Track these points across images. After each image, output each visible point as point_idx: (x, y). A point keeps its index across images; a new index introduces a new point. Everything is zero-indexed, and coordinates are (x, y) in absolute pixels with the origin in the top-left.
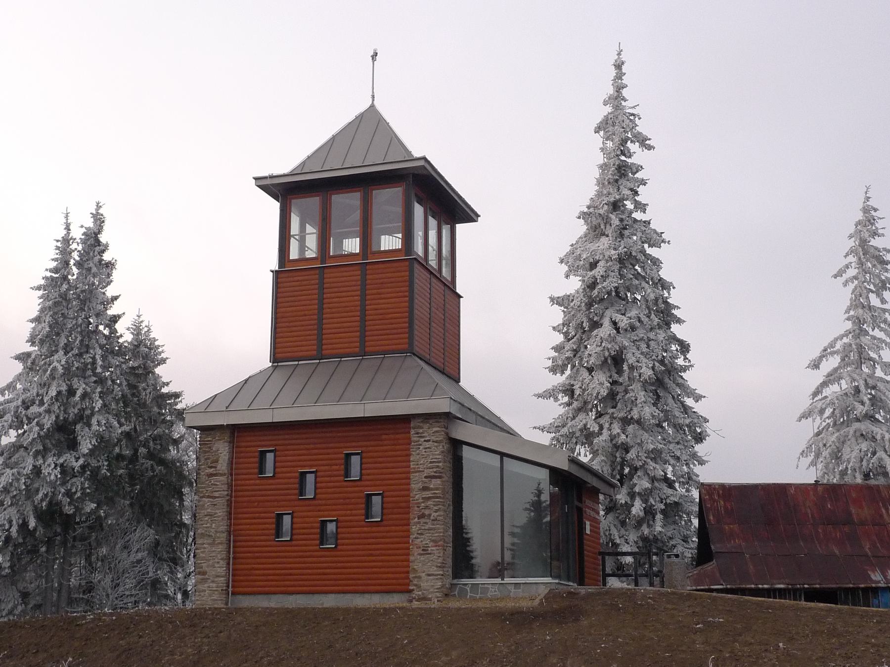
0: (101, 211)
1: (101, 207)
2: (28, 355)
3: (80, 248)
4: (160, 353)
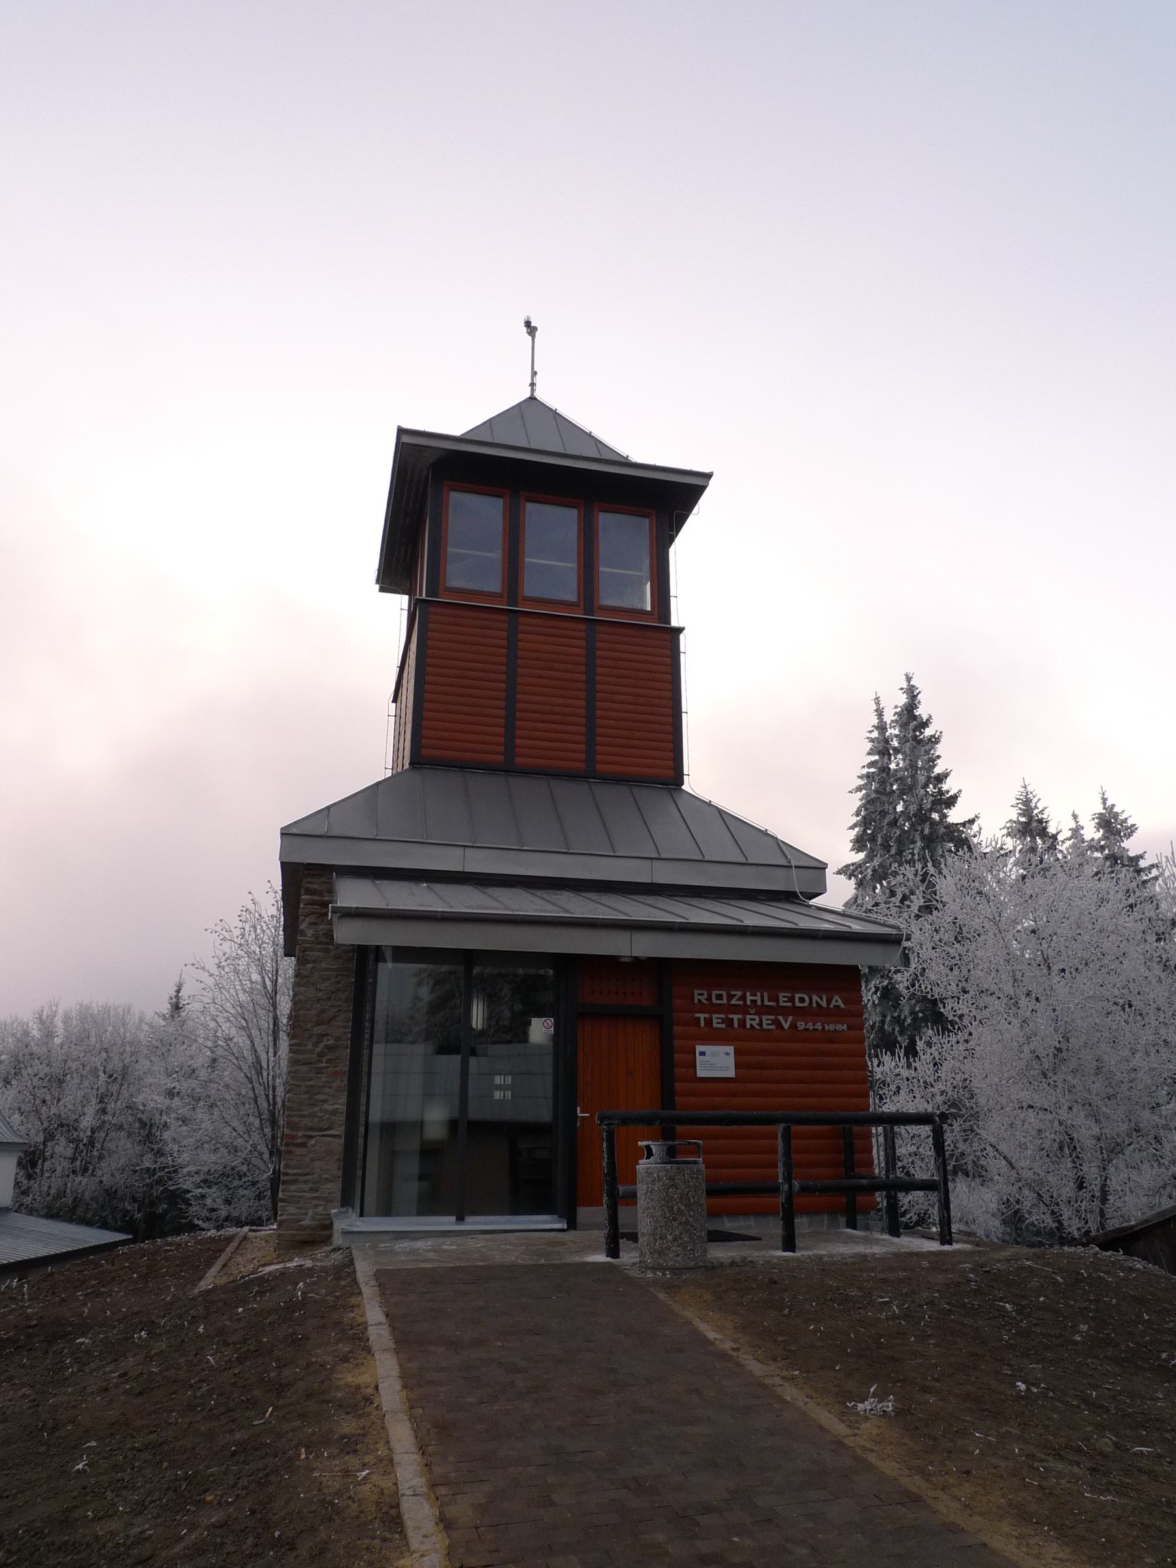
0: (912, 683)
1: (911, 678)
2: (1129, 836)
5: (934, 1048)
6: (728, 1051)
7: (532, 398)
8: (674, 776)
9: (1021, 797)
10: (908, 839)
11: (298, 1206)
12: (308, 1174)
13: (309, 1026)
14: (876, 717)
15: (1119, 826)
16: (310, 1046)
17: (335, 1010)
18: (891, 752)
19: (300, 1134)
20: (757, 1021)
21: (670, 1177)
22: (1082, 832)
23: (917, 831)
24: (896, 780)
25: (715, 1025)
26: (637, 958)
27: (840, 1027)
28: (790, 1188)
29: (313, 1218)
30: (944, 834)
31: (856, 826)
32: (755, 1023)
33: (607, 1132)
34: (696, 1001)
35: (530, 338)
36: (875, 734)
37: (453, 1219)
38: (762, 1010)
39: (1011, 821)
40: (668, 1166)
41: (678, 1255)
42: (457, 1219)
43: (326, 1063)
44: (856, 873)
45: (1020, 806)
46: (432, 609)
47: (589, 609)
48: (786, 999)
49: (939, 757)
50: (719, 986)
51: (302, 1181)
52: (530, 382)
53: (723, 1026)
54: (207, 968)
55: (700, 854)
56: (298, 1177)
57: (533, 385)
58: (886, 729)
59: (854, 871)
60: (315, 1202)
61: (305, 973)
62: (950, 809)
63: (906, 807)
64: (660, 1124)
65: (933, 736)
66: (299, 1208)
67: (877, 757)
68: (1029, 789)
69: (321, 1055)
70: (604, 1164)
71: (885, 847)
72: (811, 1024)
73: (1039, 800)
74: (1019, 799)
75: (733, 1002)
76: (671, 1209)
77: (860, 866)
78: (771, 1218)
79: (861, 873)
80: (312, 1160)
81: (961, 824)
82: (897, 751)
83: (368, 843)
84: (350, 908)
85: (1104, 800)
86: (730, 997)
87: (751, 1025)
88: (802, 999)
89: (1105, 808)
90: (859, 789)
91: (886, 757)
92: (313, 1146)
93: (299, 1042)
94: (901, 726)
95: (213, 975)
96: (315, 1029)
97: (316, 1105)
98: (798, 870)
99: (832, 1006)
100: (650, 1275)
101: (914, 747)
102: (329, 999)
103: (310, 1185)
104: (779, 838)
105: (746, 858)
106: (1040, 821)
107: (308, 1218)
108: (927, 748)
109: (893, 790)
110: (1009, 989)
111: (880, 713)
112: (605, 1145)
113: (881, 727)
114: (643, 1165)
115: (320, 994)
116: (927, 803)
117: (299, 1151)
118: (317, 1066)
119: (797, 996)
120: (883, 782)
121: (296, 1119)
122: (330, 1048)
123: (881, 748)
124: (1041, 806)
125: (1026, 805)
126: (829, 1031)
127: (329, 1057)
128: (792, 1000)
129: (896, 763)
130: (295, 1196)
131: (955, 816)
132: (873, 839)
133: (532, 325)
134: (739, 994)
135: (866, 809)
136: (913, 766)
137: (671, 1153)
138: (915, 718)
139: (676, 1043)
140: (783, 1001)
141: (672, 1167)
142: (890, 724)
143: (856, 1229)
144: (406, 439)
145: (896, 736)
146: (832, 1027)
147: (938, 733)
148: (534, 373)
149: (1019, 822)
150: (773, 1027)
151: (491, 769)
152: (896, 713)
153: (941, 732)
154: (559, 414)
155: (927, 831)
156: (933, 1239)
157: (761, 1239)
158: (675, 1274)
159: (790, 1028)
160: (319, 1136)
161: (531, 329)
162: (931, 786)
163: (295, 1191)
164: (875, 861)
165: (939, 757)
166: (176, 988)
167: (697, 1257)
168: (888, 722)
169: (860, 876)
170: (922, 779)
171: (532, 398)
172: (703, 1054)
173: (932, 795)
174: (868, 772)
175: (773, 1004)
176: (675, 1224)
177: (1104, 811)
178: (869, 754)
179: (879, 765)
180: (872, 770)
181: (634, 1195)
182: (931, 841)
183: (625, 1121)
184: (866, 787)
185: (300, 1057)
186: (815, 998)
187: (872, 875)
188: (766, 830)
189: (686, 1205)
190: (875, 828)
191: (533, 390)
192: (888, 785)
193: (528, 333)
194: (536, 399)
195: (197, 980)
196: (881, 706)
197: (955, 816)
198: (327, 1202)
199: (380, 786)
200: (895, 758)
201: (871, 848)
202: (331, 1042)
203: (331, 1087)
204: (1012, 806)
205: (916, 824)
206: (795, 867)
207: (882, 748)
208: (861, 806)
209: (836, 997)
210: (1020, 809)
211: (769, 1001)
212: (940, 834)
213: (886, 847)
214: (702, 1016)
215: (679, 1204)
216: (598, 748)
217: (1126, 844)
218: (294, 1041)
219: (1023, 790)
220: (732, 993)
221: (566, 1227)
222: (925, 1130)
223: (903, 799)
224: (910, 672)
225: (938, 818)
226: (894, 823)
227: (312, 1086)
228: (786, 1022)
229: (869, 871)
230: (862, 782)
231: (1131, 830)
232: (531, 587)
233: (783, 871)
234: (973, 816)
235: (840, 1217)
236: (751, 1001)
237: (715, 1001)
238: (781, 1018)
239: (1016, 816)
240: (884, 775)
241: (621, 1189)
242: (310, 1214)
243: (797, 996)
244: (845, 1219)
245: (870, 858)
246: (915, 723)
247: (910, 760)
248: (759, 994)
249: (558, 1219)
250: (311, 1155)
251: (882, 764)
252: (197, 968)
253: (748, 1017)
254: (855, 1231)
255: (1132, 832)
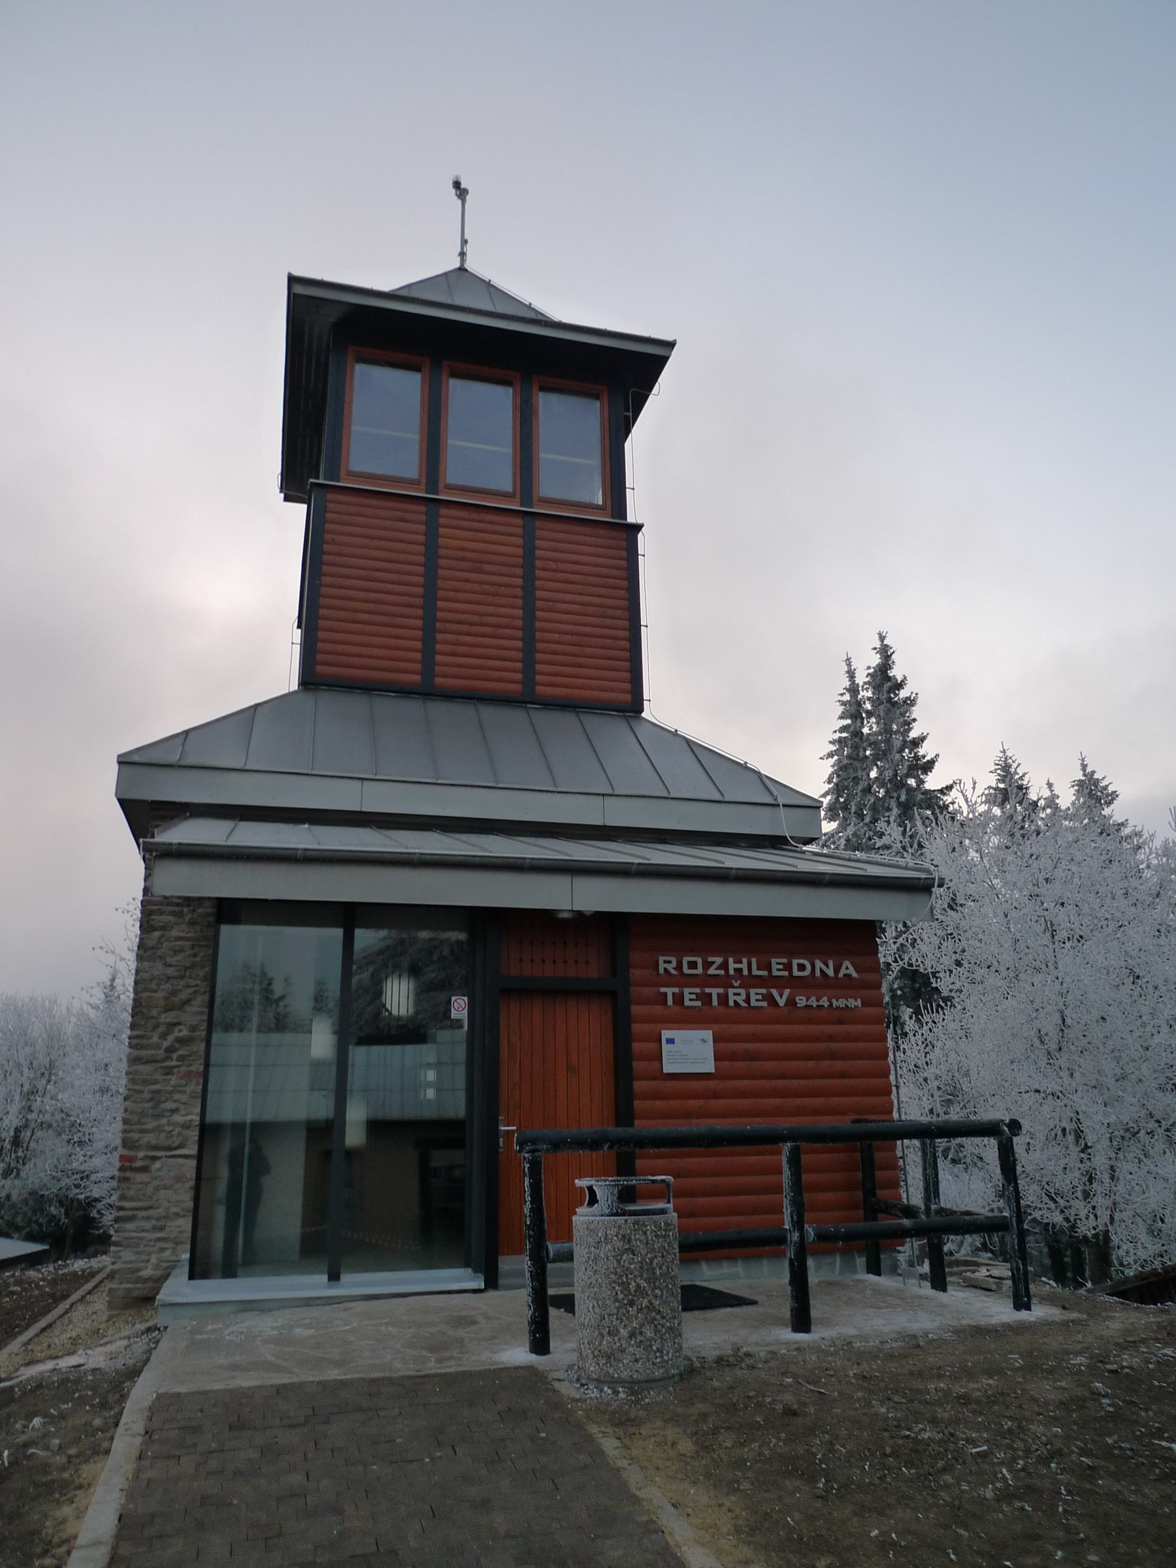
0: (885, 642)
1: (884, 637)
2: (1109, 803)
3: (870, 694)
4: (1106, 788)
5: (925, 1027)
6: (705, 1038)
7: (462, 269)
8: (634, 705)
9: (1000, 763)
10: (883, 806)
11: (135, 1250)
12: (151, 1208)
13: (154, 1012)
14: (848, 679)
15: (1099, 794)
16: (155, 1039)
17: (191, 990)
18: (864, 715)
19: (141, 1154)
20: (744, 996)
21: (624, 1236)
22: (1057, 801)
23: (893, 798)
24: (870, 745)
25: (687, 1003)
26: (580, 913)
27: (852, 1003)
28: (802, 1237)
29: (157, 1267)
30: (922, 800)
31: (828, 794)
32: (740, 1000)
33: (530, 1162)
34: (661, 971)
35: (460, 202)
36: (847, 697)
37: (324, 1278)
38: (751, 982)
39: (990, 787)
40: (620, 1220)
41: (637, 1361)
42: (330, 1279)
43: (178, 1060)
44: (828, 843)
45: (999, 771)
46: (330, 496)
47: (527, 498)
48: (781, 967)
49: (914, 720)
50: (693, 951)
51: (143, 1218)
52: (459, 250)
53: (699, 1003)
54: (117, 951)
55: (664, 789)
56: (135, 1213)
57: (462, 254)
58: (858, 691)
59: (826, 841)
60: (160, 1245)
61: (151, 943)
62: (927, 774)
63: (881, 773)
64: (610, 1148)
65: (908, 698)
66: (137, 1253)
67: (849, 721)
68: (1009, 754)
69: (170, 1050)
70: (526, 1211)
71: (858, 815)
72: (813, 999)
73: (1019, 765)
74: (998, 765)
75: (712, 971)
76: (625, 1286)
77: (833, 836)
78: (765, 1262)
79: (834, 843)
80: (157, 1189)
81: (938, 790)
82: (870, 714)
83: (233, 775)
84: (170, 844)
85: (1084, 767)
86: (707, 965)
87: (735, 1002)
88: (803, 966)
89: (1084, 775)
90: (830, 755)
91: (859, 720)
92: (159, 1170)
93: (142, 1033)
94: (874, 688)
95: (124, 959)
96: (163, 1016)
97: (164, 1116)
98: (786, 809)
99: (841, 975)
100: (594, 1393)
101: (889, 710)
102: (182, 977)
103: (154, 1222)
104: (762, 772)
105: (722, 794)
106: (1020, 787)
107: (150, 1266)
108: (902, 710)
109: (866, 756)
110: (1007, 958)
111: (851, 675)
112: (527, 1183)
113: (853, 690)
114: (582, 1216)
115: (171, 971)
116: (903, 770)
117: (139, 1177)
118: (163, 1064)
119: (795, 962)
120: (855, 748)
121: (136, 1136)
122: (182, 1041)
123: (853, 711)
124: (1020, 771)
125: (1006, 770)
126: (838, 1008)
127: (181, 1052)
128: (788, 967)
129: (869, 727)
130: (133, 1238)
131: (933, 782)
132: (845, 807)
133: (462, 186)
134: (719, 960)
135: (838, 776)
136: (887, 731)
137: (627, 1195)
138: (889, 679)
139: (636, 1027)
140: (777, 964)
141: (626, 1221)
142: (863, 686)
143: (879, 1274)
144: (299, 289)
145: (869, 699)
146: (842, 1003)
147: (914, 695)
148: (464, 242)
149: (996, 789)
150: (764, 1004)
151: (405, 692)
152: (869, 674)
153: (917, 694)
154: (493, 286)
155: (903, 798)
156: (990, 1290)
157: (753, 1303)
158: (633, 1393)
159: (786, 1005)
160: (166, 1157)
161: (460, 190)
162: (907, 750)
163: (134, 1231)
164: (848, 830)
165: (914, 720)
166: (110, 977)
167: (667, 1362)
168: (861, 684)
169: (832, 846)
170: (897, 740)
171: (462, 269)
172: (671, 1041)
173: (908, 760)
174: (840, 737)
175: (764, 973)
176: (633, 1311)
177: (1084, 778)
178: (841, 718)
179: (852, 729)
180: (844, 735)
181: (569, 1257)
182: (906, 810)
183: (557, 1145)
184: (838, 753)
185: (142, 1053)
186: (819, 964)
187: (846, 845)
188: (746, 763)
189: (648, 1281)
190: (848, 795)
191: (463, 261)
192: (861, 750)
193: (456, 195)
194: (466, 270)
195: (107, 966)
196: (852, 668)
197: (933, 782)
198: (176, 1244)
199: (258, 708)
200: (868, 722)
201: (844, 817)
202: (185, 1033)
203: (184, 1092)
204: (991, 772)
205: (890, 790)
206: (784, 805)
207: (854, 711)
208: (833, 773)
209: (847, 963)
210: (999, 775)
211: (758, 969)
212: (917, 801)
213: (861, 816)
214: (670, 991)
215: (638, 1280)
216: (539, 667)
217: (1106, 811)
218: (135, 1033)
219: (1002, 755)
220: (710, 959)
221: (483, 1287)
222: (989, 1148)
223: (877, 765)
224: (884, 630)
225: (914, 785)
226: (868, 790)
227: (158, 1091)
228: (781, 997)
229: (843, 842)
230: (833, 748)
231: (1114, 796)
232: (455, 472)
233: (769, 810)
234: (951, 782)
235: (856, 1257)
236: (735, 969)
237: (686, 971)
238: (774, 992)
239: (995, 783)
240: (857, 740)
241: (552, 1248)
242: (153, 1260)
243: (795, 962)
244: (864, 1259)
245: (843, 827)
246: (889, 684)
247: (885, 724)
248: (745, 960)
249: (473, 1274)
250: (155, 1183)
251: (855, 728)
252: (107, 952)
253: (731, 991)
254: (877, 1278)
255: (1113, 799)
